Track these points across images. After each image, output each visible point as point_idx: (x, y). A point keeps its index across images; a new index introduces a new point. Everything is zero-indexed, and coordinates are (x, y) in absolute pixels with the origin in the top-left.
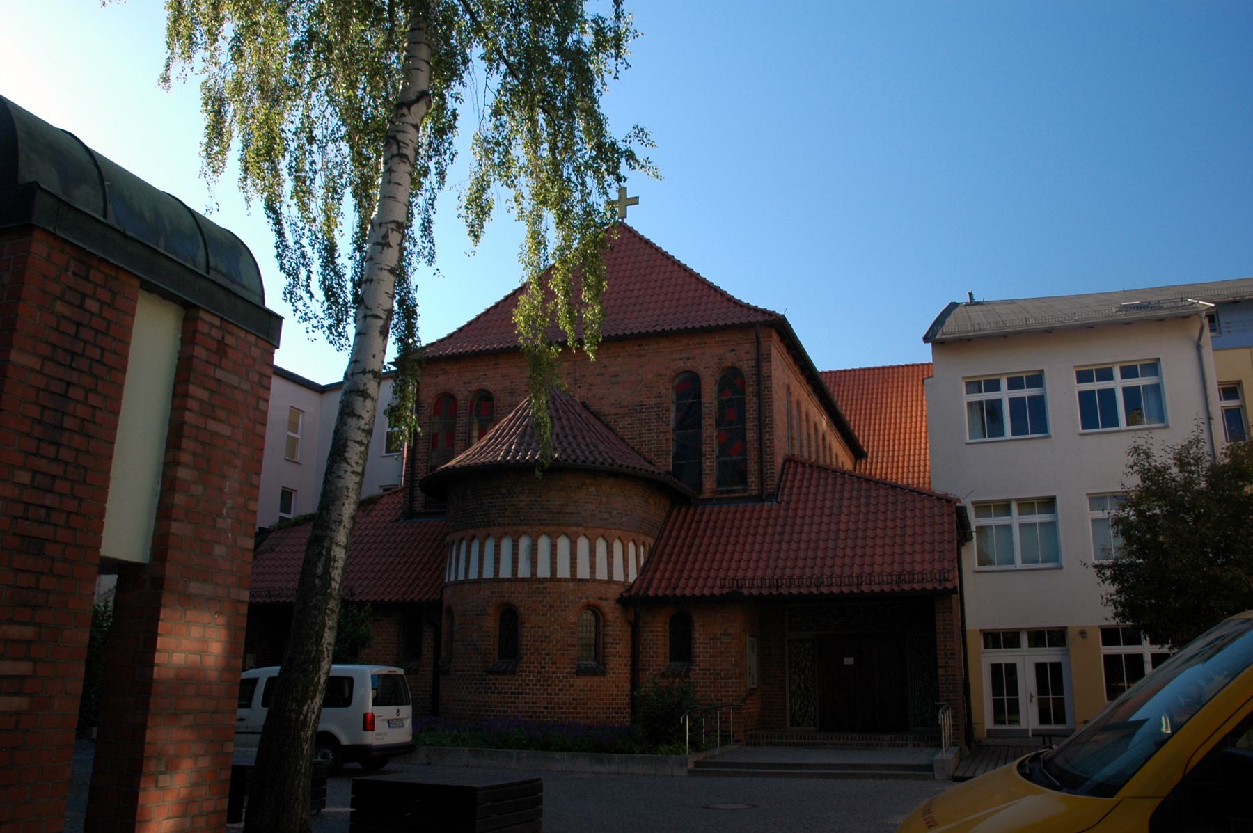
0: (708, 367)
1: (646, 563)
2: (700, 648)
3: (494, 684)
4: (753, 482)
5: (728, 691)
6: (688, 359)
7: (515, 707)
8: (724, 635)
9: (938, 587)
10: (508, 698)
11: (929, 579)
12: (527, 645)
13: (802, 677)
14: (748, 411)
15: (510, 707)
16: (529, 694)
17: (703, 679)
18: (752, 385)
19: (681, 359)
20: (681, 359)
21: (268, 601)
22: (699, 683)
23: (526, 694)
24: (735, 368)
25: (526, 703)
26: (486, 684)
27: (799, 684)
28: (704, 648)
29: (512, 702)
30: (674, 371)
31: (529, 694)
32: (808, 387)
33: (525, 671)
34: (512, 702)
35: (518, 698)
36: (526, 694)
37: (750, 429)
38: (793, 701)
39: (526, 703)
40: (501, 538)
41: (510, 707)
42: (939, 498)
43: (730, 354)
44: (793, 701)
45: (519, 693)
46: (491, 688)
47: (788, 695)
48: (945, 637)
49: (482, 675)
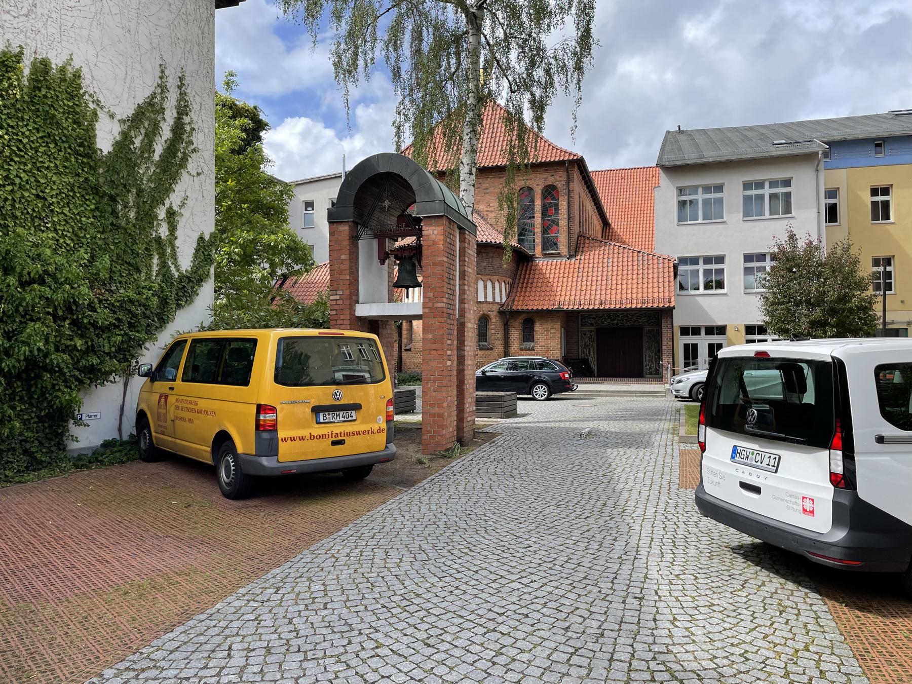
1: (510, 292)
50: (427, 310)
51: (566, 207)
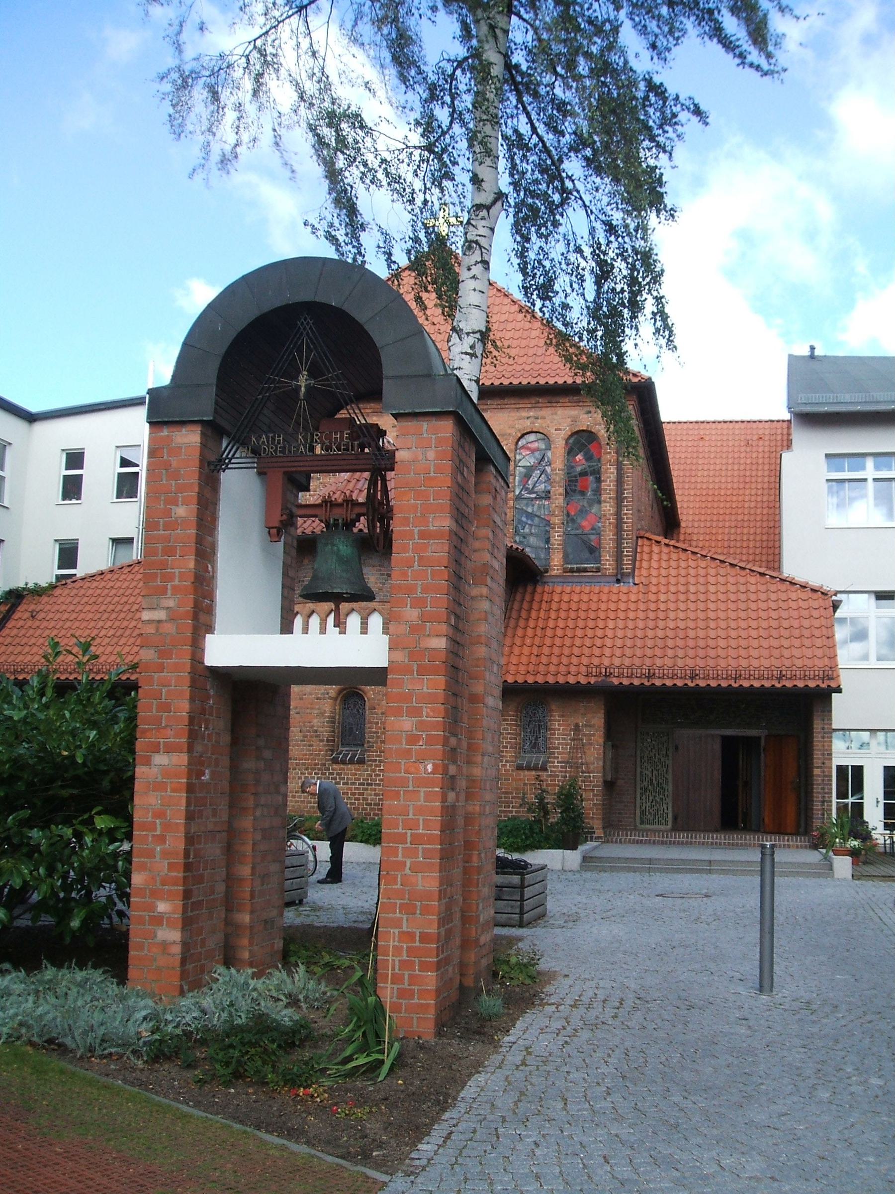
0: (560, 429)
2: (559, 739)
3: (338, 774)
4: (607, 560)
5: (506, 798)
6: (537, 418)
7: (364, 799)
8: (586, 726)
9: (646, 683)
10: (356, 789)
11: (756, 676)
12: (377, 733)
13: (655, 772)
14: (604, 481)
15: (358, 799)
16: (379, 785)
17: (561, 772)
18: (610, 453)
19: (528, 418)
20: (528, 418)
21: (778, 685)
22: (558, 776)
23: (375, 784)
24: (591, 432)
25: (376, 795)
26: (330, 774)
27: (651, 780)
28: (564, 739)
29: (360, 794)
30: (519, 431)
31: (379, 785)
32: (506, 401)
33: (375, 761)
34: (360, 794)
35: (367, 789)
36: (375, 784)
37: (605, 502)
38: (644, 797)
39: (376, 795)
40: (309, 616)
41: (358, 799)
42: (814, 590)
43: (586, 416)
44: (644, 797)
45: (368, 784)
46: (335, 779)
47: (639, 791)
48: (823, 737)
49: (324, 765)
50: (401, 657)
51: (613, 477)
